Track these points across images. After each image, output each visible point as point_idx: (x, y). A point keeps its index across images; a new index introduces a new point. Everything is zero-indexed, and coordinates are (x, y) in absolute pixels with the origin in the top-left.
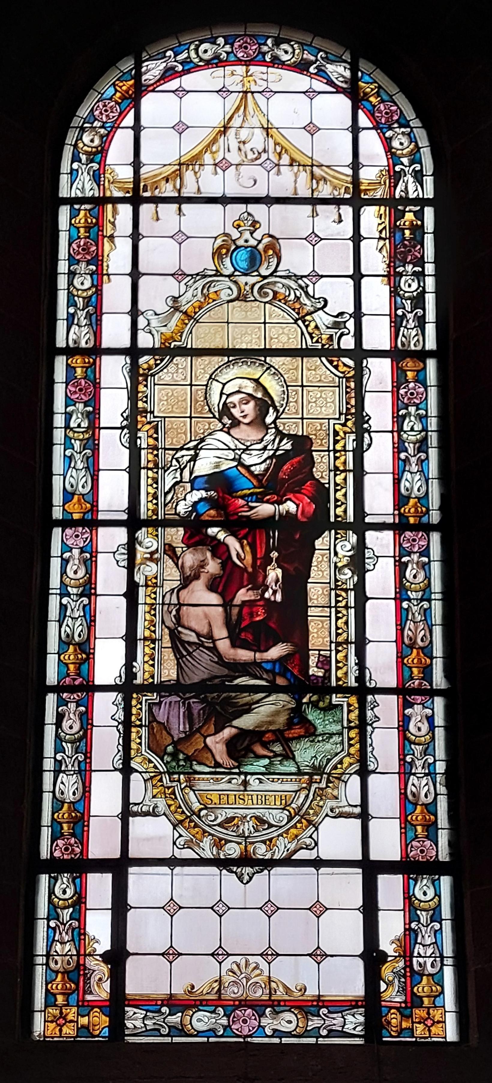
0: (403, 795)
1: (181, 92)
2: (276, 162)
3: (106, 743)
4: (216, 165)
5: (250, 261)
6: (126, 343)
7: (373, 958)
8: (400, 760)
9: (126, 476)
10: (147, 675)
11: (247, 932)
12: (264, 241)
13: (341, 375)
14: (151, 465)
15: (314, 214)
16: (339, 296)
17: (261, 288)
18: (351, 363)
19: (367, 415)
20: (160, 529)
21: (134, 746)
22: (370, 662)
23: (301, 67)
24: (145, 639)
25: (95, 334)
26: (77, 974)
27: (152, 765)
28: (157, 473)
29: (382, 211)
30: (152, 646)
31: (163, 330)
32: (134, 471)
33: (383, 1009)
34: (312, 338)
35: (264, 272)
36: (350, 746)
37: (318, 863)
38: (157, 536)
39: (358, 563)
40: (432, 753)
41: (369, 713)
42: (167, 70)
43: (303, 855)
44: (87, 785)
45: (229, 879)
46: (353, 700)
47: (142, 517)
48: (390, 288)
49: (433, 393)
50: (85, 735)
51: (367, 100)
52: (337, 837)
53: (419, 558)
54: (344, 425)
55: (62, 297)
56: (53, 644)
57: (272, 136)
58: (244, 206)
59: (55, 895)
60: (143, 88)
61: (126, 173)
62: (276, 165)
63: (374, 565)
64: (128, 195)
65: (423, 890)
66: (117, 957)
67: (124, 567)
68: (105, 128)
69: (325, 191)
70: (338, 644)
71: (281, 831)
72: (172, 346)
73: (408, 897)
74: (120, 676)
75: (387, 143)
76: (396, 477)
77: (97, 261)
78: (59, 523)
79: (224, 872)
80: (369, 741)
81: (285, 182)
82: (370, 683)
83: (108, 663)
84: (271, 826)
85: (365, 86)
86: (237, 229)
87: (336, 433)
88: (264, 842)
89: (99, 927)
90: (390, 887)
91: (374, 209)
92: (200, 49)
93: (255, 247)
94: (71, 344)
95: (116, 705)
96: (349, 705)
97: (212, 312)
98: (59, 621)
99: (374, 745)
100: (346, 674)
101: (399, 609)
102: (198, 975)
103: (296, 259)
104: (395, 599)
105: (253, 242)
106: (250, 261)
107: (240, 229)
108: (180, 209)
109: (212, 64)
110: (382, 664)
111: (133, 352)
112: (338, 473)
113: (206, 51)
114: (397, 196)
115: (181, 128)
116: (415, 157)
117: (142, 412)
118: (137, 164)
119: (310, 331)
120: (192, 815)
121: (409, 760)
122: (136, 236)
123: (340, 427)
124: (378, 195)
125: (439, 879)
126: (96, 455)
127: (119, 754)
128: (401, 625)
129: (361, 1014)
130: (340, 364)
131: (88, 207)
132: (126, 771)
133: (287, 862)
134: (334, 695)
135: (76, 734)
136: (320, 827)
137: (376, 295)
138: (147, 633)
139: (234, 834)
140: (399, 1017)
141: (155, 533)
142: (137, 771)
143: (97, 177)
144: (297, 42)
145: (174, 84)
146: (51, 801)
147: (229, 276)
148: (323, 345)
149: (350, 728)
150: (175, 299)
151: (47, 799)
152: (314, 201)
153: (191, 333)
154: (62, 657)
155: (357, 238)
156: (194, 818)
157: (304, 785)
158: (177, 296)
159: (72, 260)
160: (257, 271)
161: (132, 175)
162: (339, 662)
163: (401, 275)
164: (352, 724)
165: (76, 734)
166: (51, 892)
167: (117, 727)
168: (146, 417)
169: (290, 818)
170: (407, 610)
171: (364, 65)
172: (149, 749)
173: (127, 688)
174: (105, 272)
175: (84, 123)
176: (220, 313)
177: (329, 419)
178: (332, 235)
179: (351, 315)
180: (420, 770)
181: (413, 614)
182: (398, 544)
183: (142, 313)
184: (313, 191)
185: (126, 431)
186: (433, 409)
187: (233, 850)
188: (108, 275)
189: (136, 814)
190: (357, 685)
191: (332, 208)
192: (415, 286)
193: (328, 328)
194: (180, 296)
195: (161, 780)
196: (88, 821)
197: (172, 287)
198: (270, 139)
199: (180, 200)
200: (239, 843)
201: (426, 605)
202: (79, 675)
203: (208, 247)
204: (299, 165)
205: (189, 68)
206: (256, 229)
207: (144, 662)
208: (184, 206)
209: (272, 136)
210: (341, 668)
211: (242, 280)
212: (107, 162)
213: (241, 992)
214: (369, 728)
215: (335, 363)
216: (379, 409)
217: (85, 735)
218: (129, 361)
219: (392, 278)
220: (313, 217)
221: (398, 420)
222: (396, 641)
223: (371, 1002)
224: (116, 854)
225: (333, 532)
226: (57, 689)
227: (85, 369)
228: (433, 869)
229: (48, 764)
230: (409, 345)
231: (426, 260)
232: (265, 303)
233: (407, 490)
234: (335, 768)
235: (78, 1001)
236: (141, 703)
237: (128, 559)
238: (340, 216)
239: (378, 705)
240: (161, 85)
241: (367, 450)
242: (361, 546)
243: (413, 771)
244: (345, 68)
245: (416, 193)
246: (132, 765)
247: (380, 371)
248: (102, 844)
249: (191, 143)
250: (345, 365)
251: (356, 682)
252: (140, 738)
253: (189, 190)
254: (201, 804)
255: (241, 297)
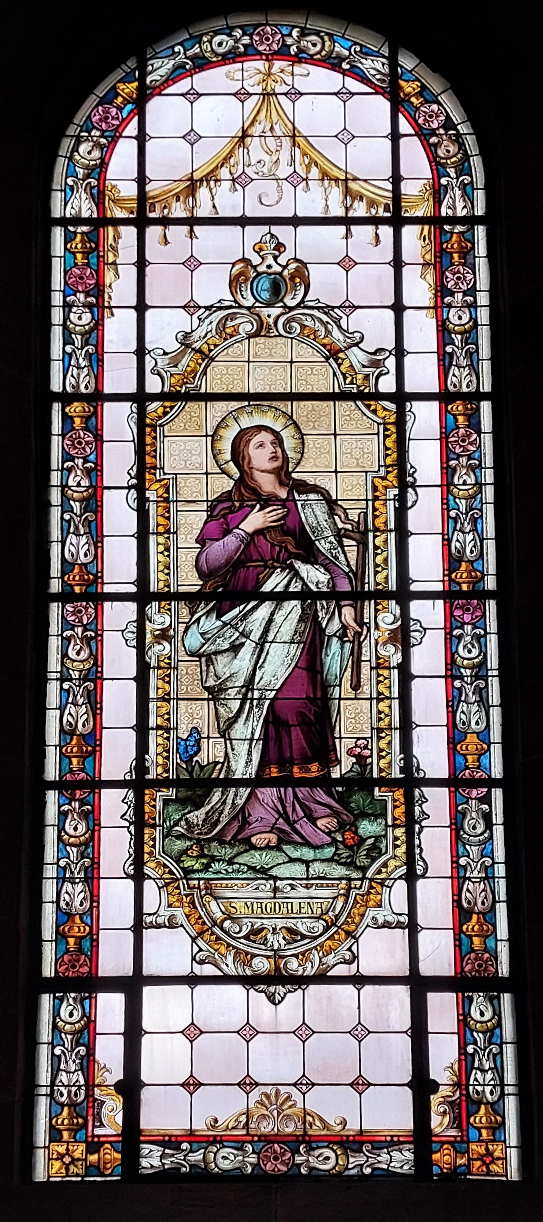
0: (457, 902)
1: (193, 96)
2: (305, 177)
3: (115, 846)
4: (234, 180)
5: (274, 288)
6: (131, 388)
7: (421, 1085)
8: (452, 862)
9: (134, 541)
10: (161, 585)
11: (274, 1061)
12: (289, 267)
13: (380, 421)
14: (161, 529)
15: (348, 235)
16: (376, 329)
17: (289, 321)
18: (392, 406)
19: (412, 467)
20: (173, 603)
21: (147, 849)
22: (416, 750)
23: (332, 62)
24: (159, 727)
25: (96, 378)
26: (85, 1110)
27: (167, 870)
28: (168, 538)
29: (426, 232)
30: (165, 735)
31: (174, 370)
32: (142, 535)
33: (434, 1145)
34: (345, 378)
35: (291, 303)
36: (396, 846)
37: (359, 980)
38: (170, 610)
39: (403, 637)
40: (483, 627)
41: (417, 809)
42: (176, 68)
43: (341, 970)
44: (95, 893)
45: (258, 999)
46: (399, 794)
47: (152, 590)
48: (437, 322)
49: (488, 441)
50: (92, 838)
51: (409, 101)
52: (382, 951)
53: (468, 460)
54: (384, 478)
55: (57, 334)
56: (52, 735)
57: (299, 146)
58: (268, 227)
59: (60, 1018)
60: (148, 92)
61: (129, 190)
62: (304, 180)
63: (421, 639)
64: (131, 216)
65: (480, 1008)
66: (130, 1087)
67: (134, 647)
68: (105, 138)
69: (360, 210)
70: (380, 730)
71: (315, 943)
72: (183, 391)
73: (464, 1021)
74: (131, 772)
75: (431, 150)
76: (446, 537)
77: (98, 290)
78: (56, 597)
79: (252, 991)
80: (417, 842)
81: (313, 201)
82: (418, 774)
83: (117, 756)
84: (304, 937)
85: (408, 87)
86: (258, 253)
87: (375, 488)
88: (296, 956)
89: (110, 1052)
90: (442, 1008)
91: (417, 228)
92: (214, 41)
93: (280, 274)
94: (69, 389)
95: (127, 803)
96: (394, 800)
97: (230, 349)
98: (60, 708)
99: (423, 846)
100: (387, 578)
101: (450, 688)
102: (223, 1108)
103: (325, 284)
104: (451, 877)
105: (277, 268)
106: (274, 288)
107: (261, 254)
108: (192, 231)
109: (229, 59)
110: (432, 755)
111: (140, 398)
112: (378, 534)
113: (220, 44)
114: (443, 214)
115: (192, 137)
116: (463, 168)
117: (151, 468)
118: (142, 180)
119: (344, 371)
120: (213, 926)
121: (454, 515)
122: (141, 264)
123: (380, 480)
124: (420, 213)
125: (498, 997)
126: (99, 519)
127: (131, 859)
128: (452, 706)
129: (409, 1150)
130: (379, 408)
131: (85, 229)
132: (138, 877)
133: (322, 978)
134: (377, 789)
135: (77, 1022)
136: (360, 940)
137: (421, 331)
138: (160, 721)
139: (263, 947)
140: (453, 1154)
141: (167, 607)
142: (150, 878)
143: (99, 197)
144: (327, 34)
145: (183, 86)
146: (58, 735)
147: (249, 308)
148: (359, 387)
149: (395, 826)
150: (187, 335)
151: (49, 913)
152: (347, 221)
153: (205, 374)
154: (64, 750)
155: (398, 264)
156: (216, 930)
157: (342, 892)
158: (189, 331)
159: (69, 289)
160: (282, 301)
161: (136, 193)
162: (378, 566)
163: (449, 306)
164: (398, 822)
165: (77, 1022)
166: (56, 1014)
167: (128, 828)
168: (155, 474)
169: (326, 929)
170: (459, 689)
171: (407, 62)
172: (164, 852)
173: (139, 783)
174: (106, 304)
175: (81, 131)
176: (239, 350)
177: (366, 472)
178: (366, 132)
179: (390, 352)
180: (475, 874)
181: (467, 695)
182: (449, 616)
183: (149, 352)
184: (347, 210)
185: (133, 491)
186: (488, 460)
187: (262, 965)
188: (110, 308)
189: (151, 926)
190: (402, 776)
191: (369, 229)
192: (466, 318)
193: (364, 366)
194: (192, 331)
195: (178, 888)
196: (98, 935)
197: (182, 321)
198: (297, 149)
199: (192, 222)
200: (268, 957)
201: (482, 684)
202: (83, 770)
203: (224, 275)
204: (331, 179)
205: (201, 64)
206: (280, 253)
207: (157, 754)
208: (196, 228)
209: (299, 146)
210: (384, 757)
211: (265, 312)
212: (108, 177)
213: (270, 1127)
214: (417, 827)
215: (373, 408)
216: (425, 459)
217: (92, 838)
218: (135, 410)
219: (439, 310)
220: (347, 238)
221: (448, 472)
222: (447, 726)
223: (421, 1136)
224: (128, 970)
225: (373, 602)
226: (59, 785)
227: (84, 420)
228: (492, 986)
229: (50, 871)
230: (461, 387)
231: (478, 289)
232: (292, 338)
233: (459, 552)
234: (379, 872)
235: (87, 1137)
236: (155, 800)
237: (137, 637)
238: (377, 235)
239: (427, 800)
240: (169, 86)
241: (412, 506)
242: (405, 615)
243: (467, 875)
244: (383, 64)
245: (465, 211)
246: (146, 871)
247: (425, 417)
248: (114, 958)
249: (205, 156)
250: (385, 409)
251: (401, 773)
252: (154, 840)
253: (203, 212)
254: (223, 913)
255: (261, 330)
